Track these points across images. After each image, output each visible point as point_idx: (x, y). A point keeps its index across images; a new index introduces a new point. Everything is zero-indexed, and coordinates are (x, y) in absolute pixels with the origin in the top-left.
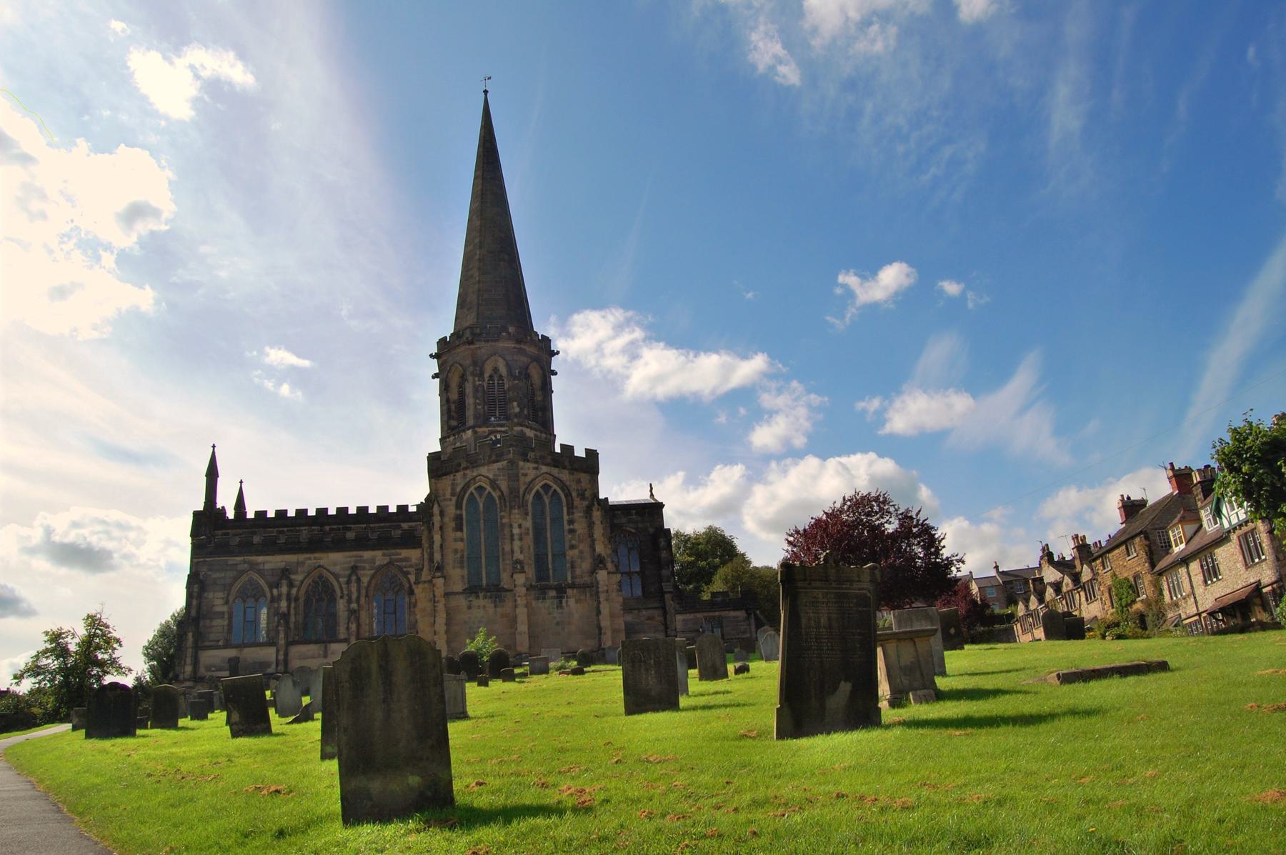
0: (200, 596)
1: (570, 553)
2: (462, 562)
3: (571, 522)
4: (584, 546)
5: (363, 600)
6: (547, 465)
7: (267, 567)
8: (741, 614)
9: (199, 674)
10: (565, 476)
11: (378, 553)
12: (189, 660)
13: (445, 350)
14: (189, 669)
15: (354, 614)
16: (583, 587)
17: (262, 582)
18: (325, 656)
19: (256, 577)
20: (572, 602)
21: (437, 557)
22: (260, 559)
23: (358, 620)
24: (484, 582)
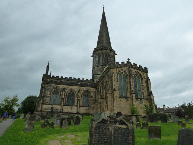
0: (44, 92)
1: (142, 90)
2: (118, 89)
3: (142, 83)
4: (146, 89)
9: (42, 110)
10: (140, 72)
11: (85, 87)
12: (40, 106)
13: (95, 51)
14: (40, 108)
15: (78, 100)
16: (146, 99)
17: (59, 91)
18: (71, 109)
21: (114, 87)
22: (59, 85)
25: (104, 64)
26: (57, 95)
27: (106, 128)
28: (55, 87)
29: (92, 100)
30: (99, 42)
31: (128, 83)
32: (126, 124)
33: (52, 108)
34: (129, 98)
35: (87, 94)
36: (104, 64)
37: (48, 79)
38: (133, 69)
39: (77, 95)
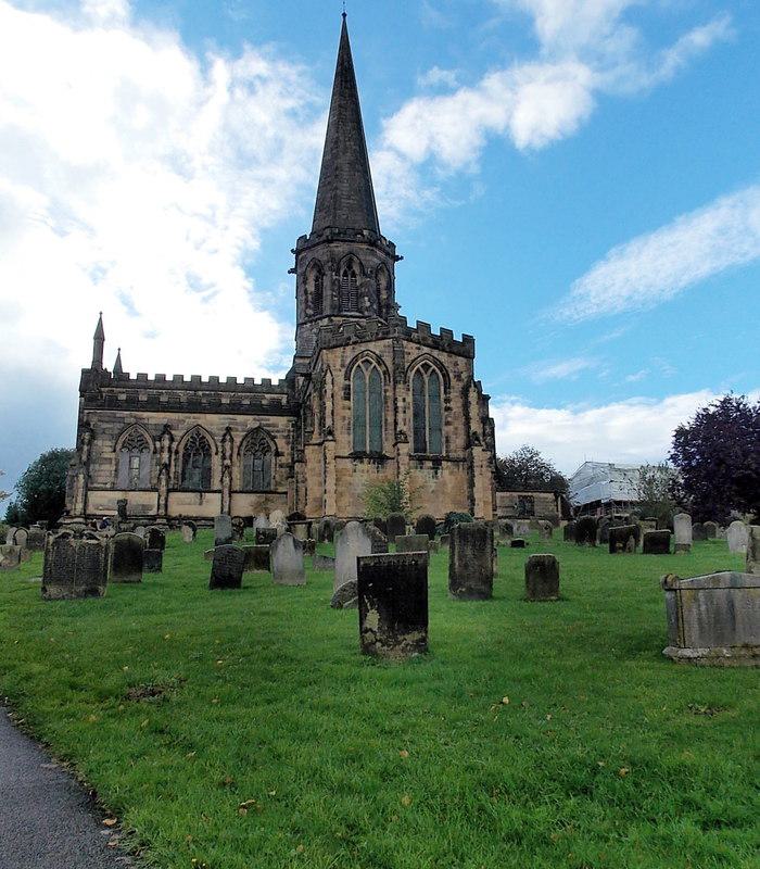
0: (90, 443)
1: (445, 429)
4: (460, 424)
5: (235, 456)
6: (428, 346)
7: (152, 422)
8: (551, 496)
9: (88, 512)
10: (443, 357)
12: (80, 499)
13: (303, 248)
14: (80, 506)
16: (456, 461)
17: (146, 435)
18: (201, 504)
19: (141, 431)
20: (446, 472)
21: (328, 422)
22: (145, 414)
23: (230, 474)
24: (368, 448)
25: (338, 310)
26: (141, 451)
27: (68, 544)
28: (133, 420)
29: (281, 466)
30: (320, 207)
31: (390, 404)
32: (97, 539)
33: (122, 506)
34: (388, 458)
35: (258, 441)
36: (338, 310)
37: (105, 390)
38: (411, 348)
39: (220, 450)
